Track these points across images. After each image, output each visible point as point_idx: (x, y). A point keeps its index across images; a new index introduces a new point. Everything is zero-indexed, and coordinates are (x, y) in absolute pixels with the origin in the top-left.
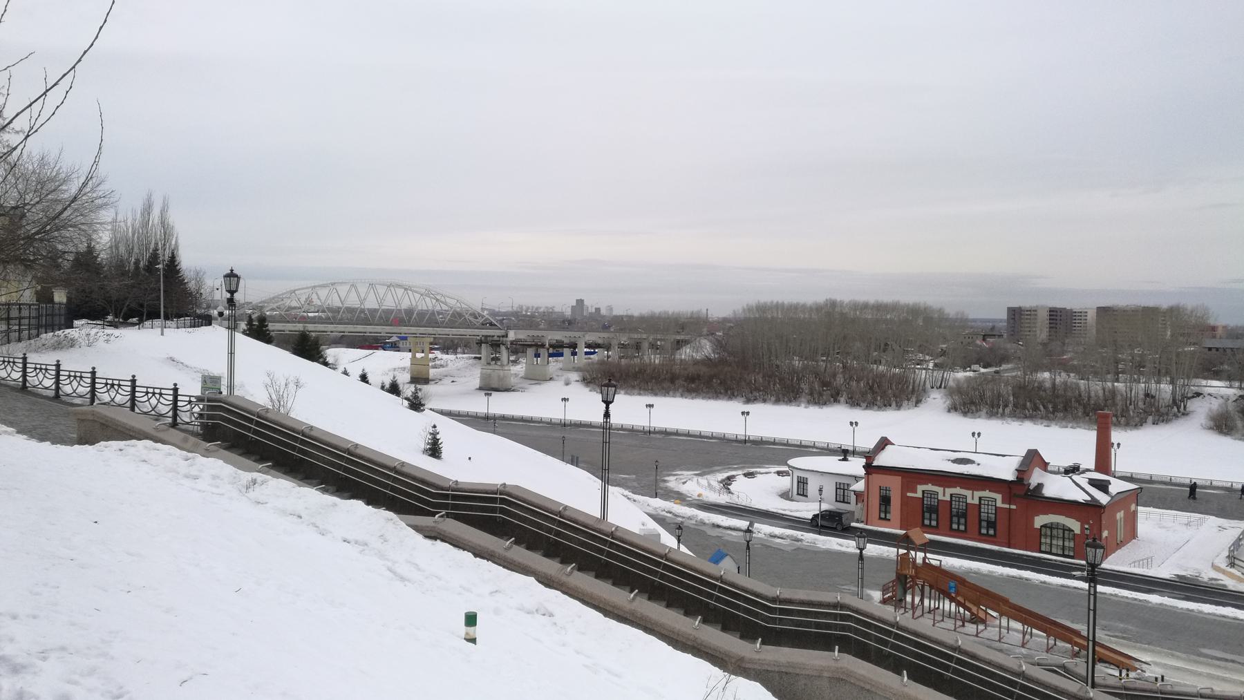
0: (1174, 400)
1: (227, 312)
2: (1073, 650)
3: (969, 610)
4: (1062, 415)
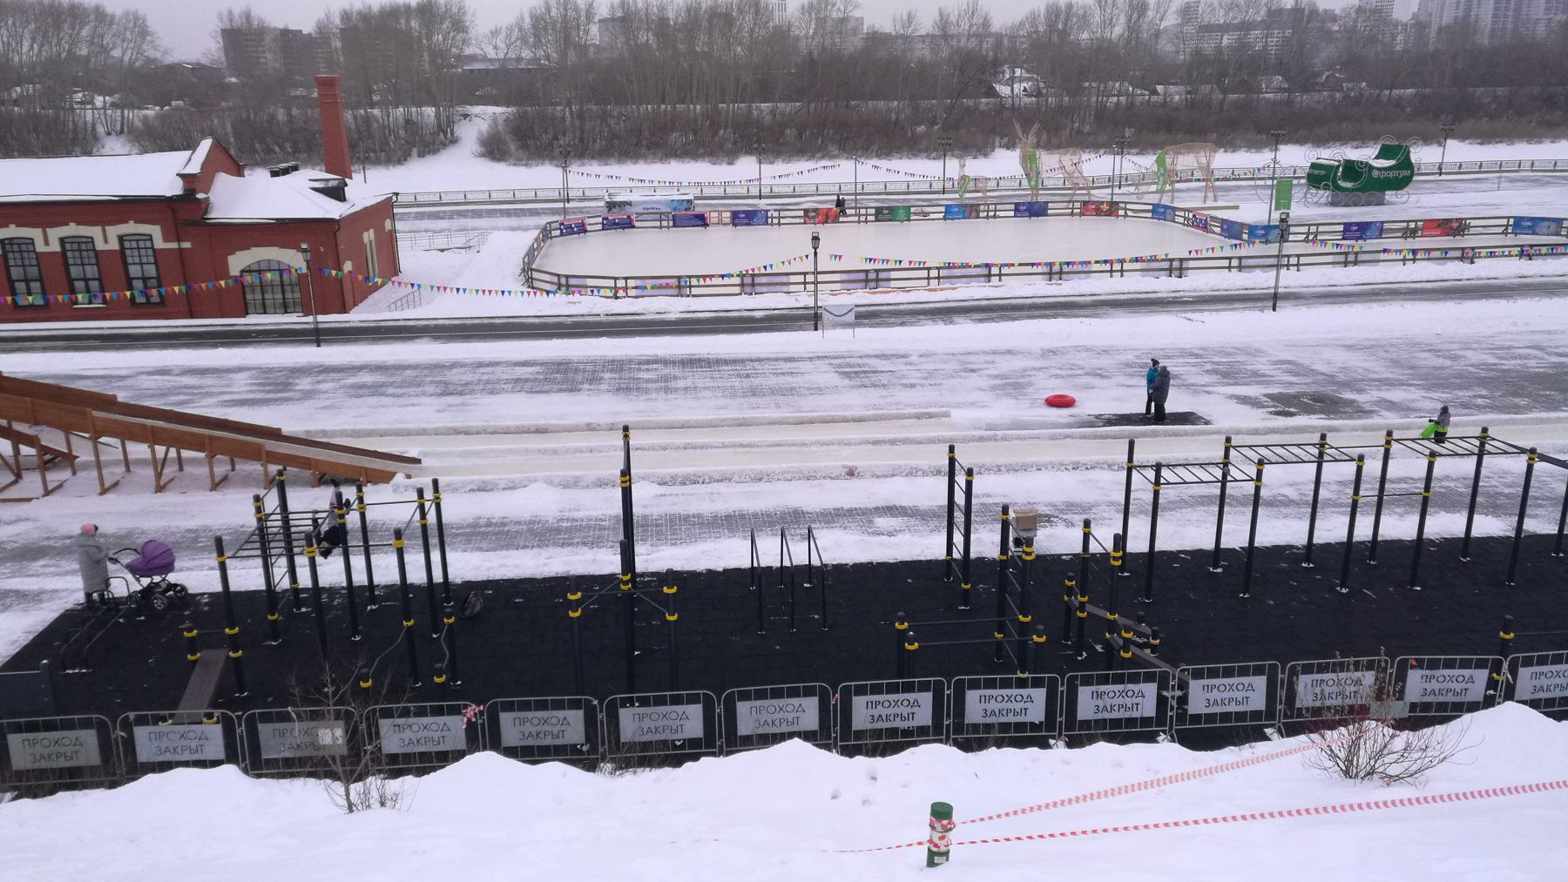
0: (439, 125)
2: (266, 472)
3: (31, 441)
4: (305, 155)
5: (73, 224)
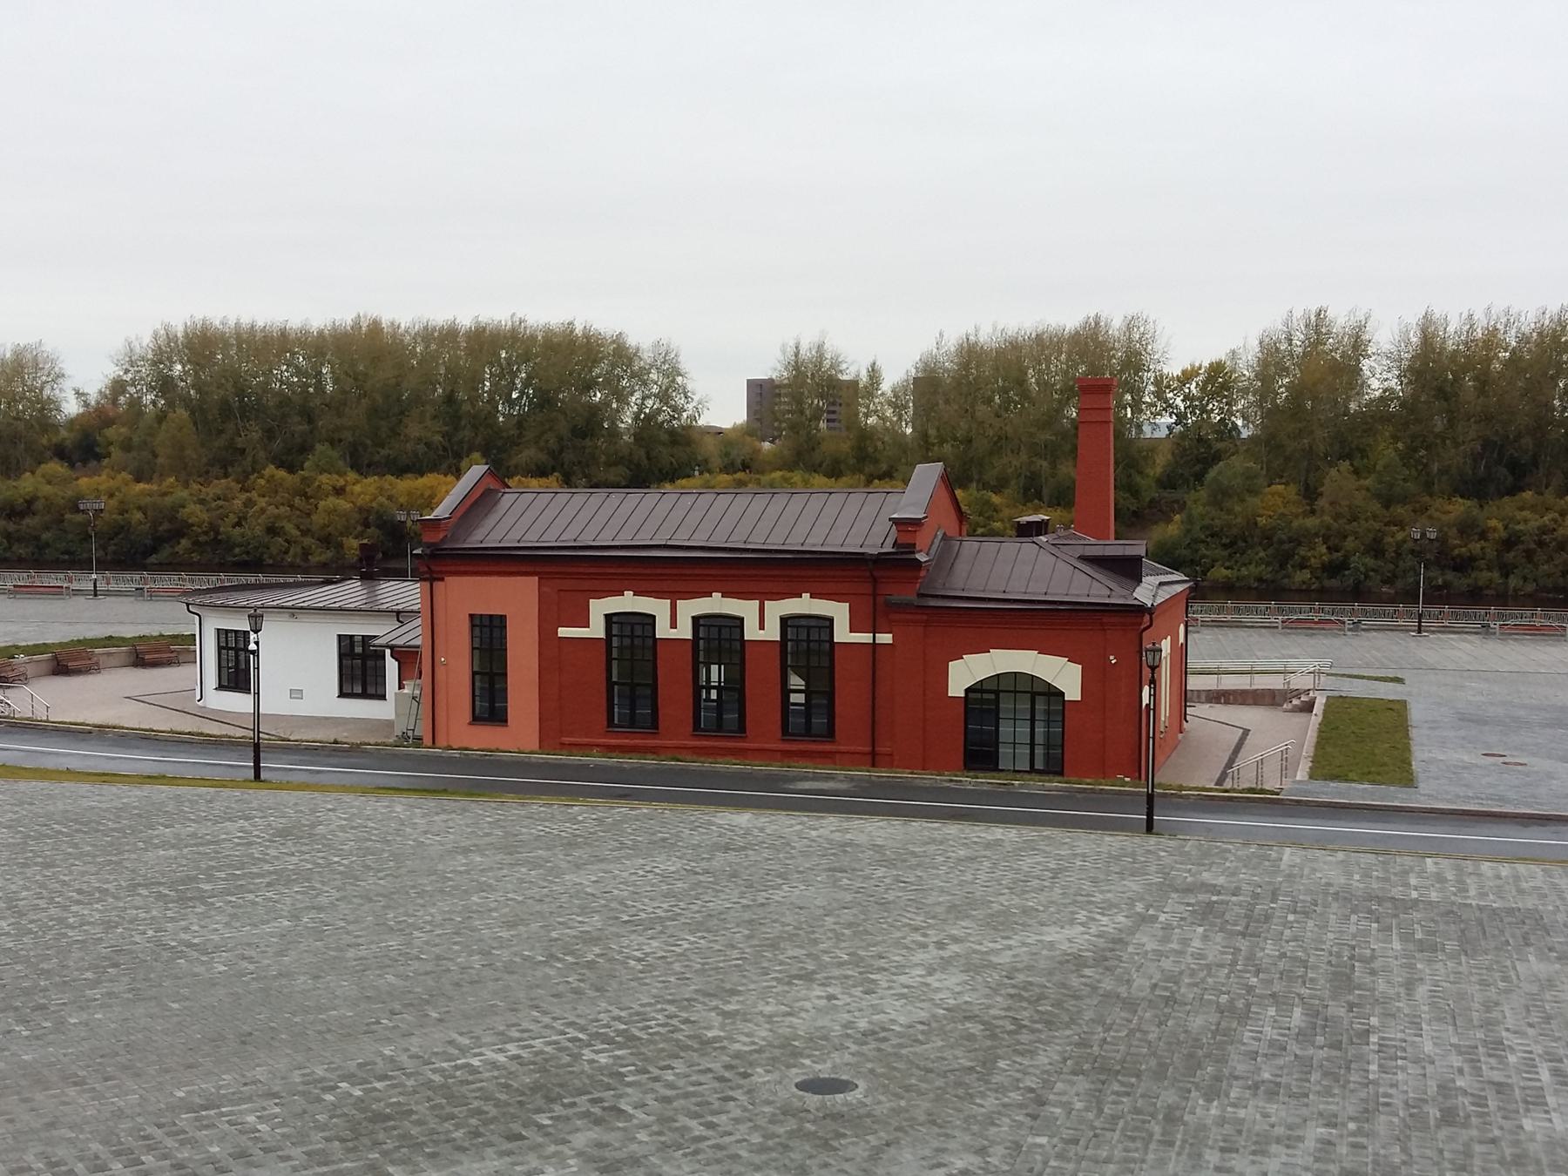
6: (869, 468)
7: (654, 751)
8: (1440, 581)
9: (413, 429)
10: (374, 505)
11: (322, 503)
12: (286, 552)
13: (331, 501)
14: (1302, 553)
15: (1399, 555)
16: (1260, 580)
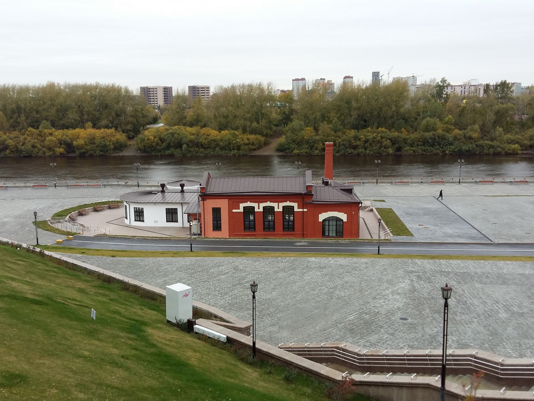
1: (309, 96)
5: (249, 202)
6: (200, 124)
7: (254, 235)
8: (350, 152)
9: (71, 116)
10: (63, 138)
11: (47, 138)
12: (38, 153)
13: (49, 138)
14: (316, 146)
15: (339, 145)
16: (306, 153)
